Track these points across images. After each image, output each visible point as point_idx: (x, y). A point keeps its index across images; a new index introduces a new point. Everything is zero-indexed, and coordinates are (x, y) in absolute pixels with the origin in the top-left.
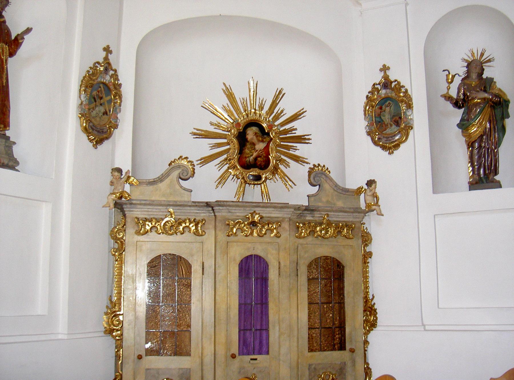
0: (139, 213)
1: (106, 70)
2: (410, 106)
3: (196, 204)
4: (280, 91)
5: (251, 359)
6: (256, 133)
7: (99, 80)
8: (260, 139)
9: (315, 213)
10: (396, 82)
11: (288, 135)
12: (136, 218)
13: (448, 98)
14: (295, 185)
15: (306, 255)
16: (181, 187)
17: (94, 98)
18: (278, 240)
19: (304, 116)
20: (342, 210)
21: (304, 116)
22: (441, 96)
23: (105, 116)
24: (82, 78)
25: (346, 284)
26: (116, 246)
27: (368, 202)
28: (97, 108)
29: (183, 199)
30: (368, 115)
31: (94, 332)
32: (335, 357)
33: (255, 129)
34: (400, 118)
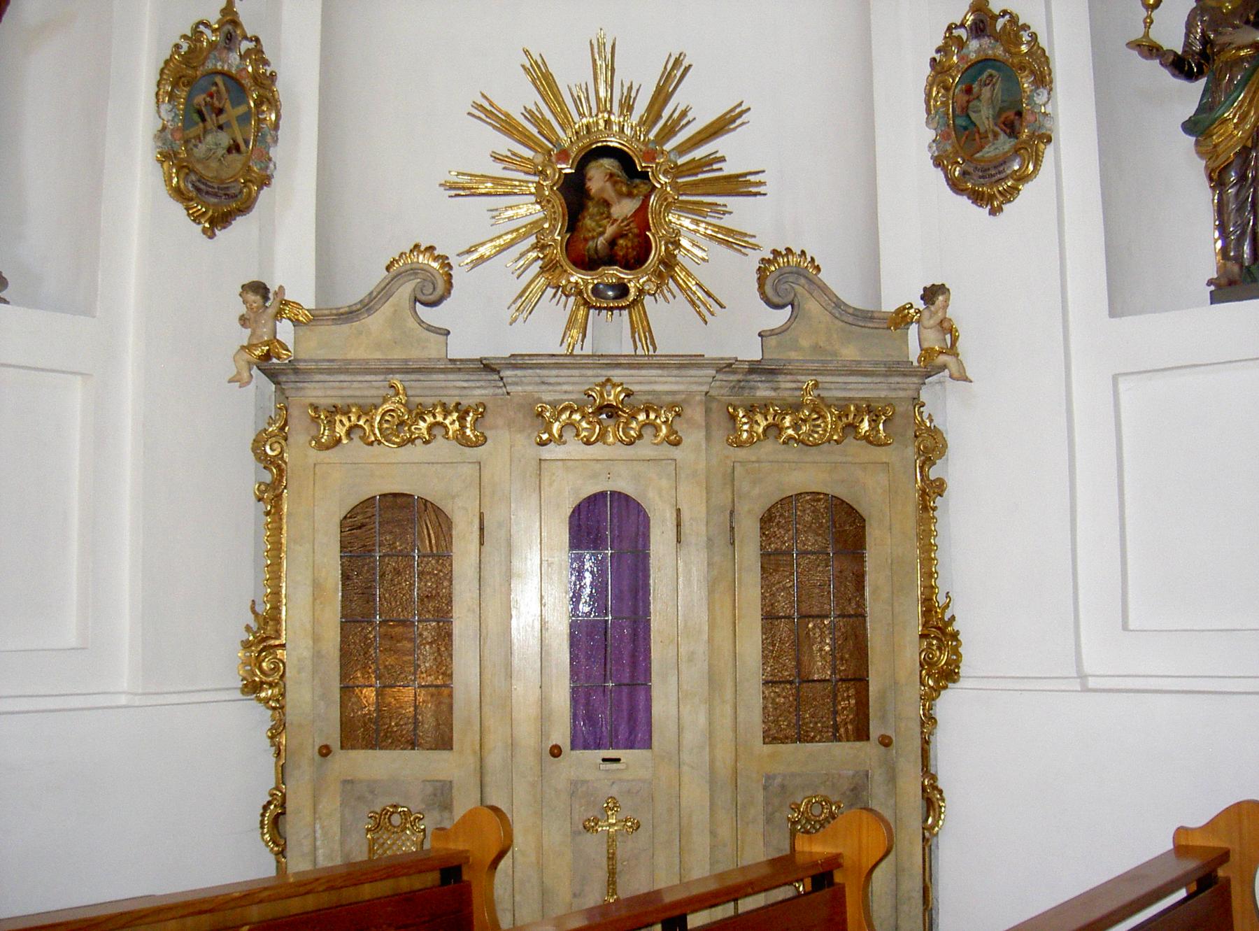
0: (319, 392)
1: (230, 40)
2: (1043, 80)
3: (457, 366)
4: (677, 60)
5: (604, 760)
6: (612, 175)
7: (209, 65)
8: (624, 189)
9: (780, 378)
10: (1007, 17)
11: (701, 176)
12: (311, 405)
13: (1150, 50)
14: (722, 306)
15: (756, 491)
16: (421, 322)
17: (200, 113)
18: (676, 452)
19: (743, 124)
20: (853, 370)
21: (743, 124)
22: (1129, 45)
23: (235, 155)
24: (162, 65)
25: (869, 566)
26: (268, 478)
27: (926, 345)
28: (209, 138)
29: (425, 354)
30: (937, 112)
31: (216, 690)
32: (839, 757)
33: (608, 164)
34: (1019, 114)
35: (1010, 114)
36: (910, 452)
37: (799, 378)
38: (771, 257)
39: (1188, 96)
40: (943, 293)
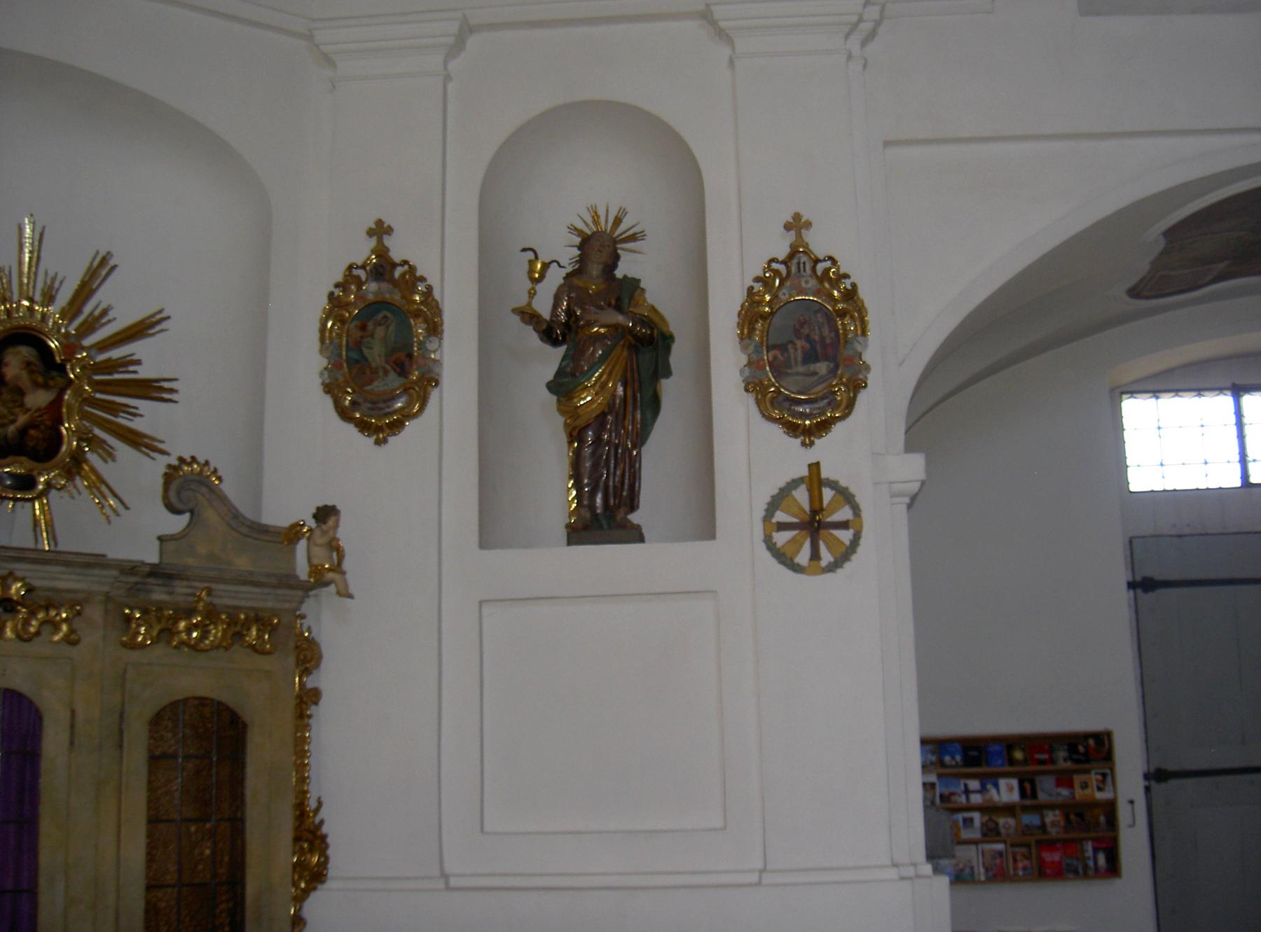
2: (435, 329)
6: (28, 364)
8: (40, 379)
10: (406, 267)
11: (116, 376)
13: (528, 316)
14: (127, 508)
18: (74, 651)
22: (515, 311)
27: (316, 561)
33: (25, 351)
34: (410, 356)
35: (402, 355)
36: (291, 660)
37: (195, 584)
38: (189, 460)
39: (550, 359)
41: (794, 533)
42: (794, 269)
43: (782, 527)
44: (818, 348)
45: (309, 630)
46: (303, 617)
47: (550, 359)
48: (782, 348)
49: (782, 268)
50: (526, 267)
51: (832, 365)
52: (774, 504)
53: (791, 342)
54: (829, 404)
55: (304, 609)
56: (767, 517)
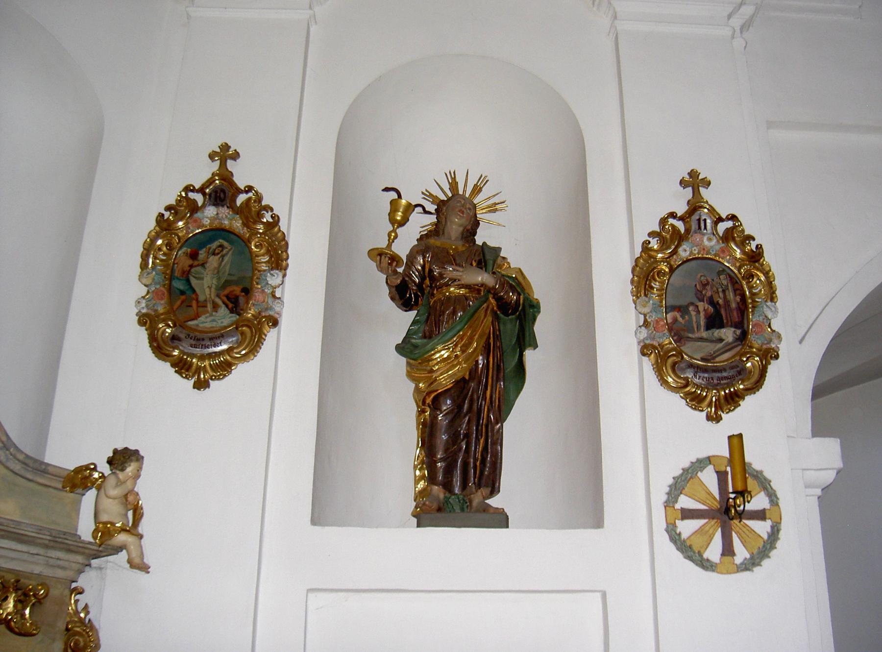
2: (279, 262)
27: (104, 518)
33: (396, 197)
34: (247, 291)
35: (237, 290)
39: (403, 321)
40: (138, 460)
41: (702, 522)
42: (694, 226)
43: (687, 514)
44: (723, 312)
45: (86, 608)
46: (81, 592)
47: (403, 321)
48: (682, 309)
49: (680, 225)
50: (388, 208)
51: (738, 332)
52: (677, 488)
53: (692, 304)
54: (739, 373)
55: (81, 583)
56: (669, 503)
